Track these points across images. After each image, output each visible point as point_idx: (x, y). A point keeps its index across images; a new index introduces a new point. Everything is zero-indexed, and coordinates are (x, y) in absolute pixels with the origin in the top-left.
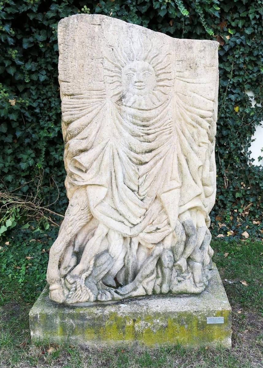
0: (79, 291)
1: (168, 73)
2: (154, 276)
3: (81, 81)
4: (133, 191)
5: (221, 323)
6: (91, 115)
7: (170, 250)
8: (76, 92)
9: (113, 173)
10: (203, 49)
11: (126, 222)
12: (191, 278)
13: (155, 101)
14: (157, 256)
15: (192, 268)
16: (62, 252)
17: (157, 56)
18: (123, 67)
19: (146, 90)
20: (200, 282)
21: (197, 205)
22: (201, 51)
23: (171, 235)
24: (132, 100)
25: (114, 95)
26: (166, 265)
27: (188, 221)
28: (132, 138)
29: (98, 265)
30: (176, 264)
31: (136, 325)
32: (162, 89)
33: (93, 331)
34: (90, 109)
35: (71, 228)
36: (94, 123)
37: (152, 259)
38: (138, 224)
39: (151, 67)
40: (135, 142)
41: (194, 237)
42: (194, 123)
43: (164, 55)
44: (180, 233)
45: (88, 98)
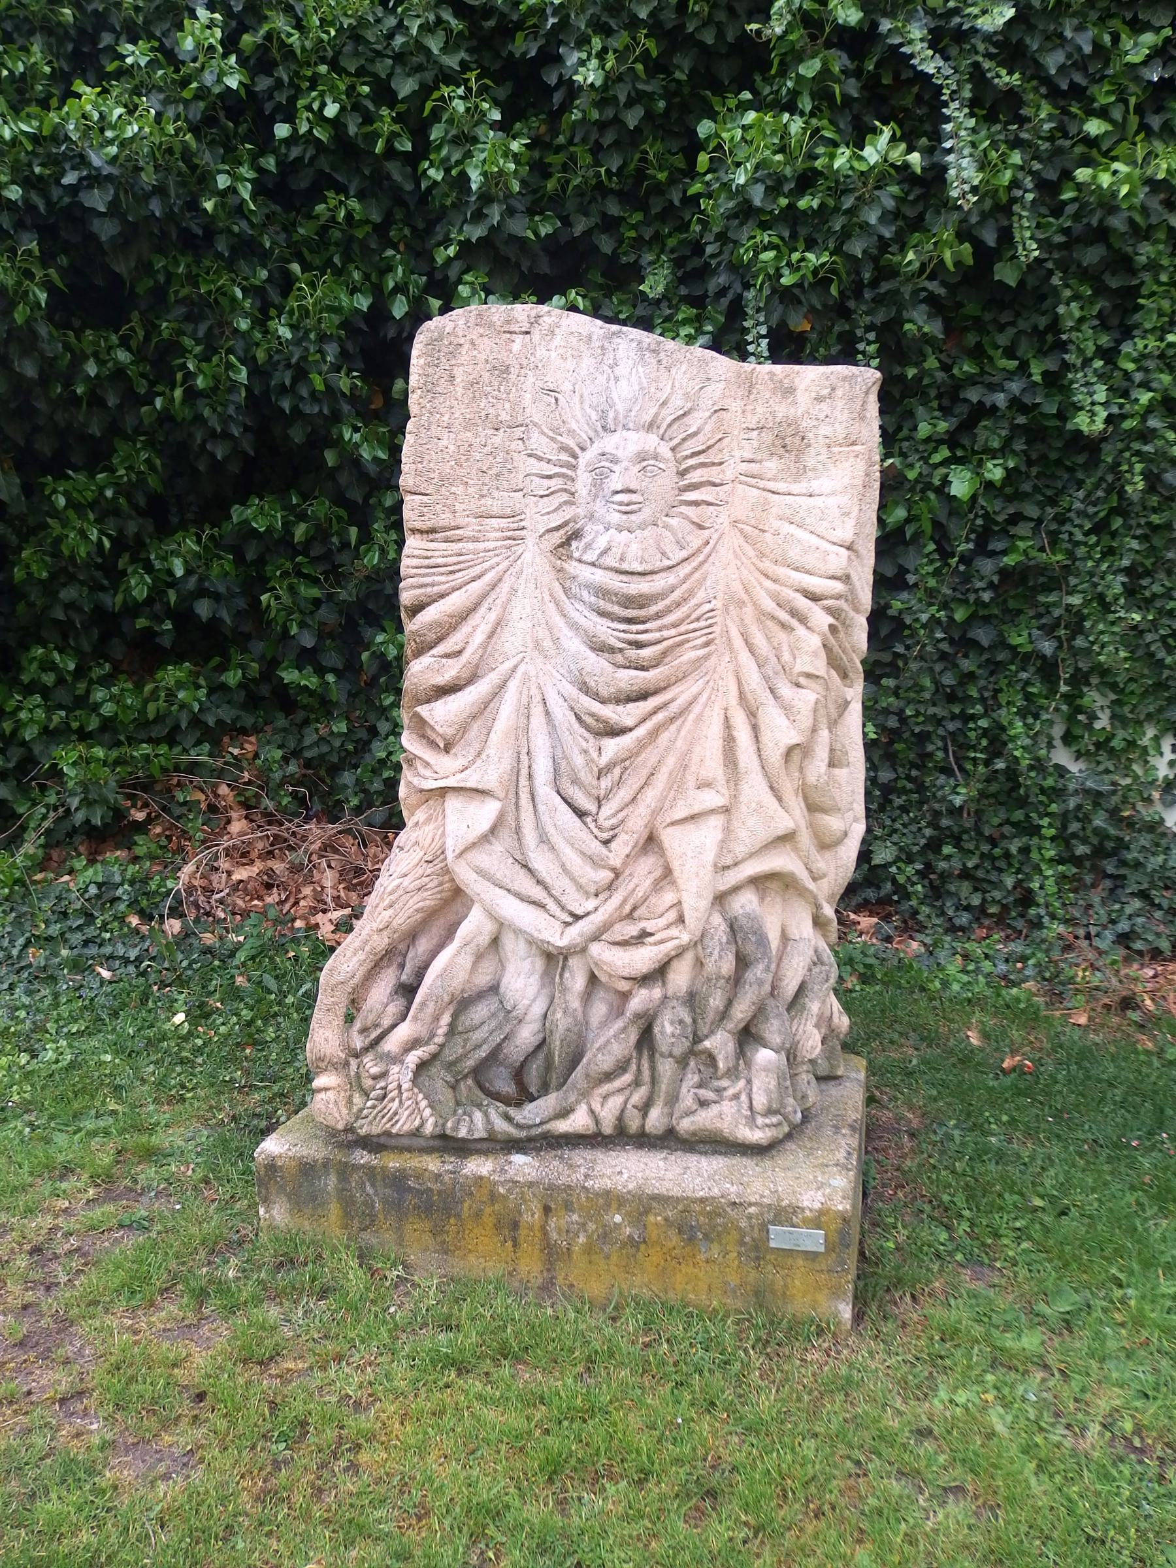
0: (393, 1100)
1: (714, 464)
2: (627, 1078)
3: (459, 490)
4: (581, 814)
5: (814, 1249)
6: (477, 587)
7: (684, 1003)
8: (442, 523)
9: (524, 757)
10: (826, 392)
11: (551, 905)
12: (743, 1097)
13: (669, 546)
14: (638, 1016)
15: (748, 1064)
16: (355, 980)
17: (684, 415)
18: (583, 449)
19: (646, 514)
20: (770, 1112)
21: (778, 869)
22: (819, 399)
23: (689, 957)
24: (602, 543)
25: (548, 531)
26: (664, 1048)
27: (748, 916)
28: (592, 655)
29: (460, 1029)
30: (700, 1047)
31: (553, 1223)
32: (690, 511)
33: (427, 1225)
34: (477, 570)
35: (390, 912)
36: (482, 610)
37: (620, 1024)
38: (588, 914)
39: (664, 450)
40: (596, 664)
41: (761, 966)
42: (784, 616)
43: (708, 414)
44: (716, 952)
45: (476, 540)
